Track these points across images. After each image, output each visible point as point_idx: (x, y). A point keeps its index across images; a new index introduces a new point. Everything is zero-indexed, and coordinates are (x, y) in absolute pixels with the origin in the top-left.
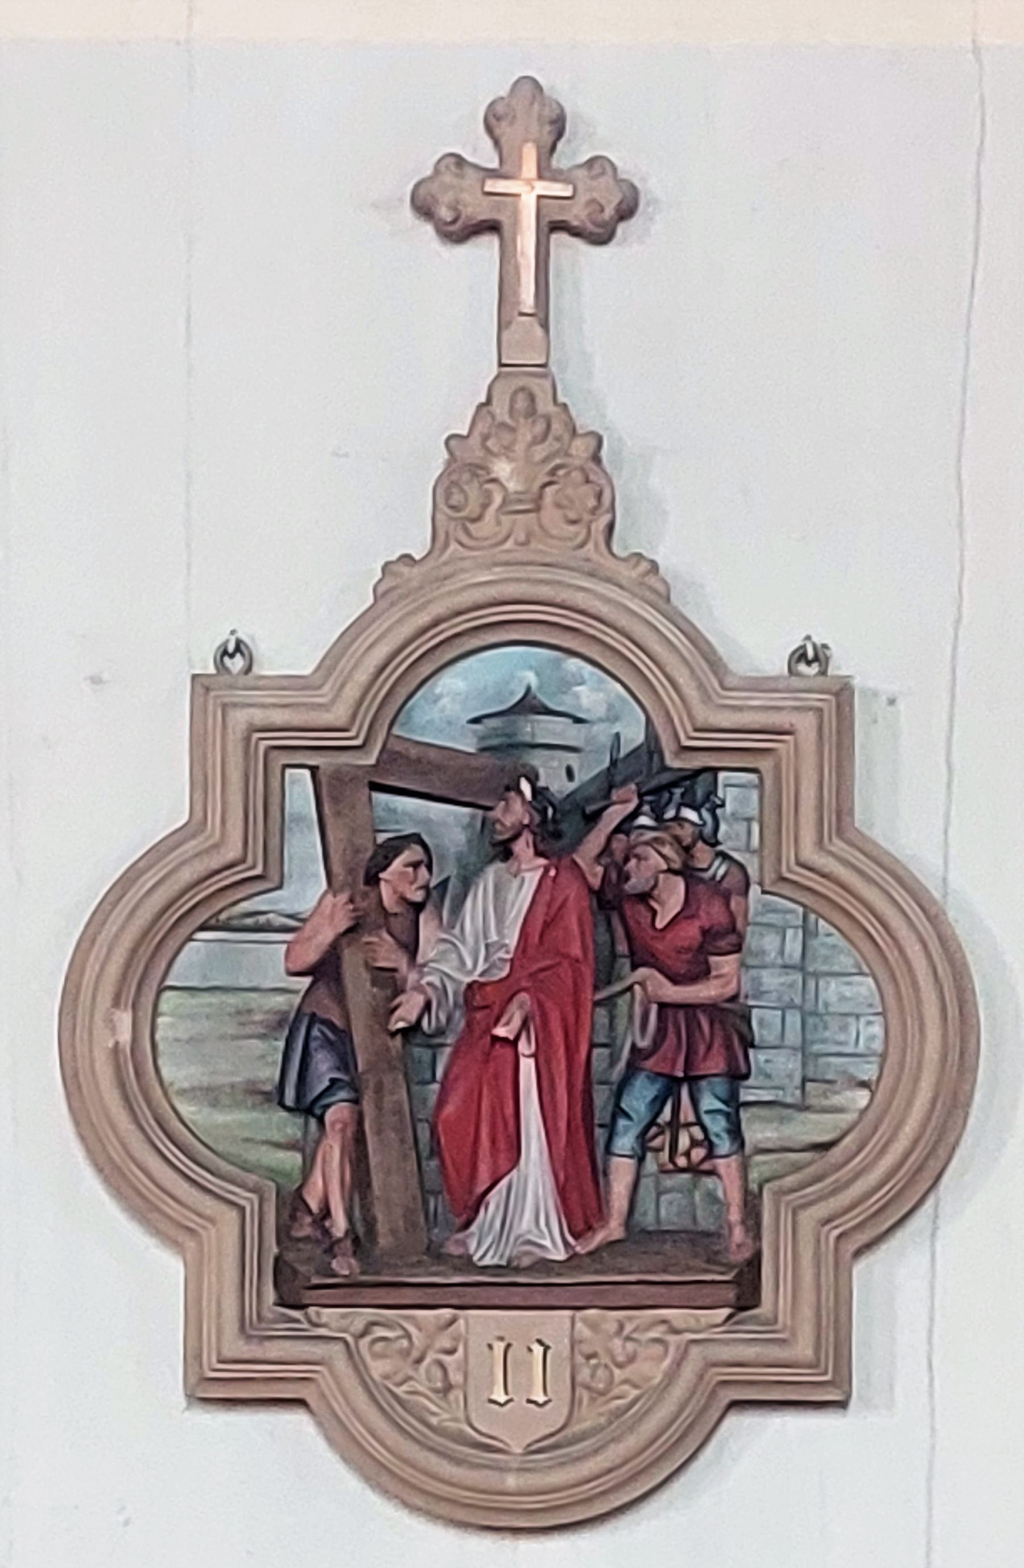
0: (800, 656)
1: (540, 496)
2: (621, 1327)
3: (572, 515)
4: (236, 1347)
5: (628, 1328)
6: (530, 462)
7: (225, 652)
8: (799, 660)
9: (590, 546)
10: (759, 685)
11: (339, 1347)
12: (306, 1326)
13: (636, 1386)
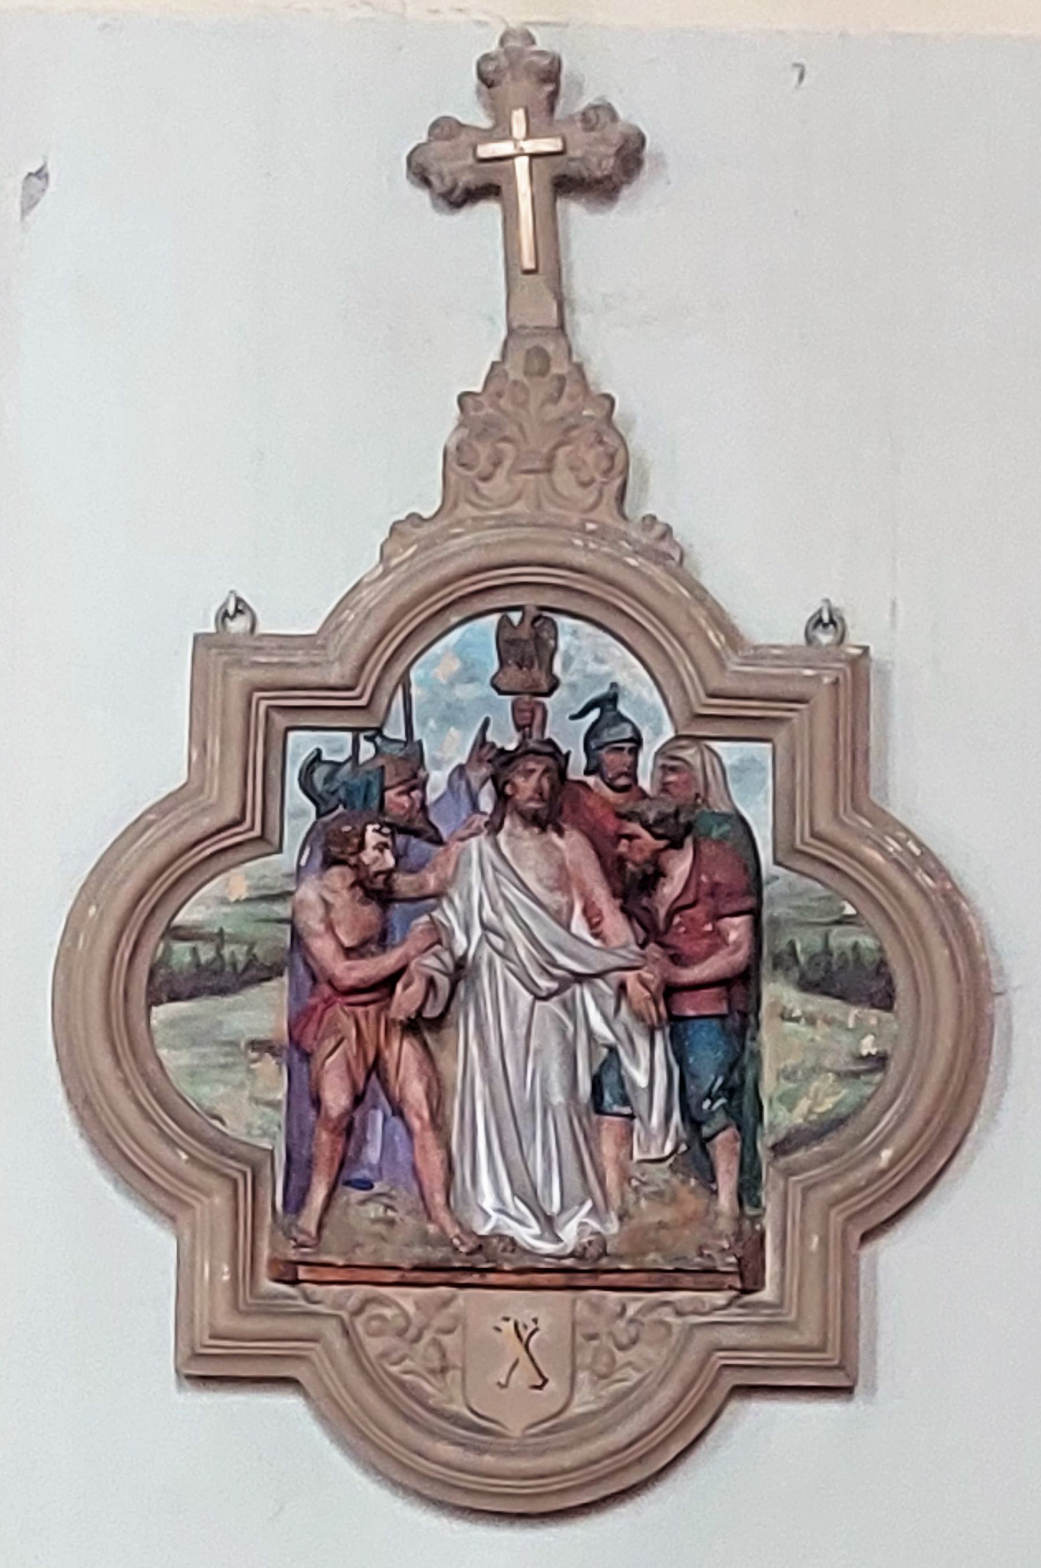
0: (818, 622)
1: (551, 459)
2: (624, 1309)
3: (586, 478)
4: (225, 1322)
5: (631, 1311)
6: (540, 412)
7: (226, 614)
8: (816, 626)
9: (602, 507)
10: (787, 656)
11: (334, 1323)
12: (302, 1302)
13: (638, 1370)
